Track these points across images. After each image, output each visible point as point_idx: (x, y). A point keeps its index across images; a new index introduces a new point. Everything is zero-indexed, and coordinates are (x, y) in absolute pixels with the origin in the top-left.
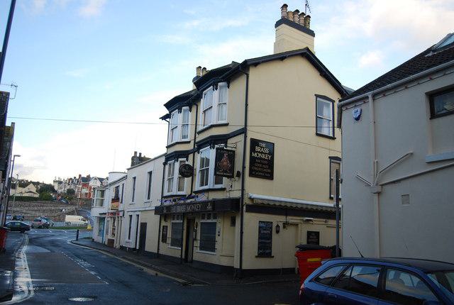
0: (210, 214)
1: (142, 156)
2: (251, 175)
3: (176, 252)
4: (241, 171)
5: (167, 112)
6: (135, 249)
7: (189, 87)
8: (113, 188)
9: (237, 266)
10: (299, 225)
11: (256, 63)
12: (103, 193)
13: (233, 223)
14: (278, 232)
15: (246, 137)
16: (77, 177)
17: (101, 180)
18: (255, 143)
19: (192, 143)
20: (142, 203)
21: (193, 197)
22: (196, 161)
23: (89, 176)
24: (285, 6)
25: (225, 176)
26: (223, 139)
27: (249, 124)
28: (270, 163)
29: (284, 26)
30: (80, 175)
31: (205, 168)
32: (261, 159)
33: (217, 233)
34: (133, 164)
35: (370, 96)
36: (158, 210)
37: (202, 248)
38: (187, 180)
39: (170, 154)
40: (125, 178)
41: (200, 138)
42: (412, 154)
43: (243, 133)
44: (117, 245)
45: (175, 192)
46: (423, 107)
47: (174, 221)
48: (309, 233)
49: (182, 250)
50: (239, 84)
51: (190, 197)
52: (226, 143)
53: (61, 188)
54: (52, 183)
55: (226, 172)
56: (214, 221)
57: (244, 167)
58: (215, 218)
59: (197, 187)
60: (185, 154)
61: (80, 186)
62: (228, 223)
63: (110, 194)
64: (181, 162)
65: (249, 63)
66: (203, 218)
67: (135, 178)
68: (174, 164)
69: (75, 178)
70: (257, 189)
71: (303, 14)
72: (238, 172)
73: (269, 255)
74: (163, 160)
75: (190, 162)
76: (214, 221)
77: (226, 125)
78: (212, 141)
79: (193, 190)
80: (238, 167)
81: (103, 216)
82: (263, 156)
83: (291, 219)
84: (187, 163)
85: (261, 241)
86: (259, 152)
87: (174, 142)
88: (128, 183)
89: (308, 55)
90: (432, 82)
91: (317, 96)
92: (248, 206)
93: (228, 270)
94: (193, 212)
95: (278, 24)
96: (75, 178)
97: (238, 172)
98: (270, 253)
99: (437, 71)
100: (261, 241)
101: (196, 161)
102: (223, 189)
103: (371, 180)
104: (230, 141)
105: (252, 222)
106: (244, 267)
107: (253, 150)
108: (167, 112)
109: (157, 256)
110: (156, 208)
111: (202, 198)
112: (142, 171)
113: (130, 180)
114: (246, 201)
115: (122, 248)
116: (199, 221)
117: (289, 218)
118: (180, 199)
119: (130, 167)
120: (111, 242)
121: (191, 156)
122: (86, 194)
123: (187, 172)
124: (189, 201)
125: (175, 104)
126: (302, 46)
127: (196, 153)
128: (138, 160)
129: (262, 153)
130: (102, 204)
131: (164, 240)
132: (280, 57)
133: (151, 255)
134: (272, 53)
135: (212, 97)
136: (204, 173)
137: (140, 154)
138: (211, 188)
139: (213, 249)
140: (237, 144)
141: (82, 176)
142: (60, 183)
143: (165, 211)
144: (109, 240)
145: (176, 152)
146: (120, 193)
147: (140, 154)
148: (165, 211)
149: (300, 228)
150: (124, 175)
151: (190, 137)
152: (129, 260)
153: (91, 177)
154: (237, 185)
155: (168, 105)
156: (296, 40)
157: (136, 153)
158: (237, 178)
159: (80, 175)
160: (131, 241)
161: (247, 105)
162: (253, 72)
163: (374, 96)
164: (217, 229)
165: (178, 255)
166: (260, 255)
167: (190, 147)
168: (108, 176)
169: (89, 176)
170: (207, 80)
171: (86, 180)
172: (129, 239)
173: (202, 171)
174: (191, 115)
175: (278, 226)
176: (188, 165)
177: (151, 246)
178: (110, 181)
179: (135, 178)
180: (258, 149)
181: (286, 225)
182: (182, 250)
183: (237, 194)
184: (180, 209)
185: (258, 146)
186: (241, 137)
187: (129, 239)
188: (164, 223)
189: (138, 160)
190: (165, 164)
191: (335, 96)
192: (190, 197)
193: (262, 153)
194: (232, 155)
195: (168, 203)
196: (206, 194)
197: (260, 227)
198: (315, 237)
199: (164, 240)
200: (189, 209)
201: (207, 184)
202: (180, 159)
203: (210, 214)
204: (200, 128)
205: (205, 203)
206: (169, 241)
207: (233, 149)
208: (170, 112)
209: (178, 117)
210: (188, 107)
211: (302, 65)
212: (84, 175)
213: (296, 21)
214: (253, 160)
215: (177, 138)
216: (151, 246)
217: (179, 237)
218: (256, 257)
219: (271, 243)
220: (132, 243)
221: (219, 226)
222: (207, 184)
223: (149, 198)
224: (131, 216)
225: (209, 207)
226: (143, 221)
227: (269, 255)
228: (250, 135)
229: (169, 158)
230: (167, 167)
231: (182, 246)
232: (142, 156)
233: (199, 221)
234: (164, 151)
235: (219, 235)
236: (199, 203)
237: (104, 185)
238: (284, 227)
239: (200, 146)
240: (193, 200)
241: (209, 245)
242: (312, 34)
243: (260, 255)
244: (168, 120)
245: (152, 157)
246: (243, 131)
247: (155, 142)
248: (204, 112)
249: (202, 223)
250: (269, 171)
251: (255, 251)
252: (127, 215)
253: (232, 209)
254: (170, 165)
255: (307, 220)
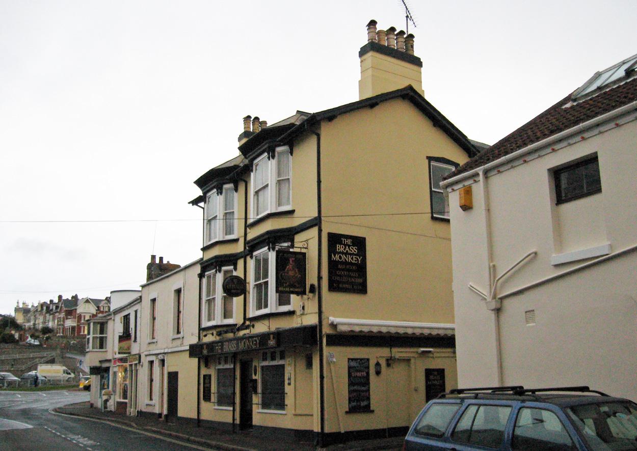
0: (227, 357)
1: (165, 262)
2: (333, 287)
3: (225, 414)
4: (316, 283)
5: (199, 192)
6: (160, 415)
7: (228, 152)
8: (119, 318)
9: (317, 429)
10: (412, 361)
11: (331, 115)
12: (103, 327)
13: (309, 365)
14: (378, 373)
15: (320, 231)
16: (56, 300)
17: (97, 302)
18: (334, 239)
19: (242, 241)
20: (169, 337)
21: (247, 327)
22: (248, 270)
23: (75, 298)
24: (373, 23)
25: (293, 293)
26: (289, 234)
27: (323, 214)
28: (361, 269)
29: (370, 55)
30: (60, 297)
31: (262, 281)
32: (346, 263)
33: (286, 382)
34: (150, 277)
35: (481, 173)
36: (194, 351)
37: (265, 405)
38: (237, 301)
39: (207, 261)
40: (140, 299)
41: (253, 234)
42: (536, 253)
43: (315, 225)
44: (131, 411)
45: (218, 320)
46: (544, 188)
47: (221, 367)
48: (429, 372)
49: (234, 410)
50: (307, 151)
51: (244, 327)
52: (292, 241)
53: (29, 321)
54: (13, 314)
55: (294, 287)
56: (281, 362)
57: (320, 278)
58: (282, 357)
59: (252, 312)
60: (232, 260)
61: (62, 315)
62: (302, 364)
63: (115, 328)
64: (226, 272)
65: (318, 118)
66: (265, 359)
67: (154, 300)
68: (215, 275)
69: (51, 301)
70: (345, 313)
71: (402, 33)
72: (312, 286)
73: (367, 409)
74: (198, 269)
75: (239, 273)
76: (281, 362)
77: (291, 212)
78: (271, 239)
79: (247, 317)
80: (311, 279)
81: (105, 365)
82: (349, 259)
83: (398, 352)
84: (235, 274)
85: (352, 388)
86: (343, 253)
87: (213, 241)
88: (144, 309)
89: (412, 97)
90: (584, 144)
91: (430, 159)
92: (328, 336)
93: (303, 435)
94: (248, 352)
95: (363, 52)
96: (51, 301)
97: (312, 286)
98: (368, 406)
99: (560, 140)
100: (352, 388)
101: (248, 270)
102: (291, 313)
103: (485, 291)
104: (299, 238)
105: (338, 359)
106: (327, 430)
107: (332, 250)
108: (199, 192)
109: (199, 422)
110: (192, 346)
111: (261, 328)
112: (165, 289)
113: (146, 303)
114: (326, 330)
115: (141, 413)
116: (259, 364)
117: (394, 350)
118: (226, 332)
119: (144, 282)
120: (122, 406)
121: (241, 263)
122: (73, 328)
123: (235, 287)
124: (242, 333)
125: (213, 180)
126: (400, 85)
127: (248, 258)
128: (159, 270)
129: (347, 254)
130: (102, 343)
131: (207, 398)
132: (369, 104)
133: (188, 421)
134: (356, 99)
135: (266, 170)
136: (262, 288)
137: (161, 259)
138: (274, 311)
139: (281, 405)
140: (309, 243)
141: (64, 298)
142: (26, 311)
143: (205, 352)
144: (119, 403)
145: (216, 257)
146: (132, 325)
147: (161, 259)
148: (205, 352)
149: (413, 367)
150: (137, 295)
151: (238, 232)
152: (154, 432)
153: (80, 297)
154: (312, 306)
155: (202, 182)
156: (396, 76)
157: (153, 257)
158: (311, 295)
159: (60, 297)
160: (154, 401)
161: (319, 182)
162: (326, 130)
163: (486, 172)
164: (286, 378)
165: (229, 420)
166: (352, 410)
167: (240, 248)
168: (109, 295)
169: (75, 298)
170: (261, 140)
171: (69, 306)
172: (151, 399)
173: (258, 287)
174: (237, 198)
175: (378, 364)
176: (237, 277)
177: (186, 408)
178: (114, 307)
179: (154, 300)
180: (340, 248)
181: (390, 362)
182: (234, 410)
183: (311, 320)
184: (230, 348)
185: (341, 243)
186: (314, 231)
187: (151, 399)
188: (204, 371)
189: (159, 270)
190: (201, 276)
191: (461, 158)
192: (244, 327)
193: (347, 254)
194: (301, 259)
195: (209, 338)
196: (266, 322)
197: (350, 368)
198: (438, 377)
199: (207, 398)
200: (241, 346)
201: (266, 306)
202: (224, 268)
203: (227, 357)
204: (252, 218)
205: (264, 337)
206: (214, 398)
207: (303, 251)
208: (205, 194)
209: (217, 200)
210: (231, 186)
211: (404, 112)
212: (67, 296)
213: (390, 46)
214: (332, 265)
215: (219, 236)
216: (186, 408)
217: (230, 391)
218: (347, 412)
219: (368, 390)
220: (159, 406)
221: (289, 371)
222: (266, 306)
223: (178, 332)
224: (151, 362)
225: (272, 342)
226: (172, 370)
227: (367, 409)
228: (327, 228)
229: (206, 266)
230: (204, 280)
231: (233, 404)
232: (165, 262)
233: (259, 364)
234: (199, 255)
235: (289, 384)
236: (257, 336)
237: (102, 313)
238: (388, 365)
239: (252, 246)
240: (247, 331)
241: (275, 399)
242: (418, 62)
243: (352, 410)
244: (202, 204)
245: (183, 265)
246: (316, 222)
247: (186, 245)
248: (257, 193)
249: (263, 367)
250: (360, 280)
251: (212, 376)
252: (145, 361)
253: (306, 341)
254: (209, 277)
255: (423, 352)
